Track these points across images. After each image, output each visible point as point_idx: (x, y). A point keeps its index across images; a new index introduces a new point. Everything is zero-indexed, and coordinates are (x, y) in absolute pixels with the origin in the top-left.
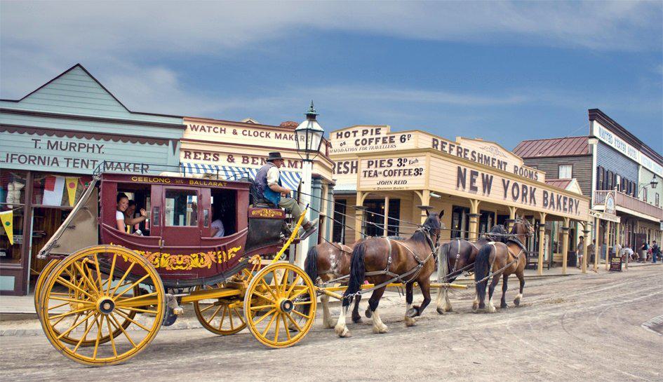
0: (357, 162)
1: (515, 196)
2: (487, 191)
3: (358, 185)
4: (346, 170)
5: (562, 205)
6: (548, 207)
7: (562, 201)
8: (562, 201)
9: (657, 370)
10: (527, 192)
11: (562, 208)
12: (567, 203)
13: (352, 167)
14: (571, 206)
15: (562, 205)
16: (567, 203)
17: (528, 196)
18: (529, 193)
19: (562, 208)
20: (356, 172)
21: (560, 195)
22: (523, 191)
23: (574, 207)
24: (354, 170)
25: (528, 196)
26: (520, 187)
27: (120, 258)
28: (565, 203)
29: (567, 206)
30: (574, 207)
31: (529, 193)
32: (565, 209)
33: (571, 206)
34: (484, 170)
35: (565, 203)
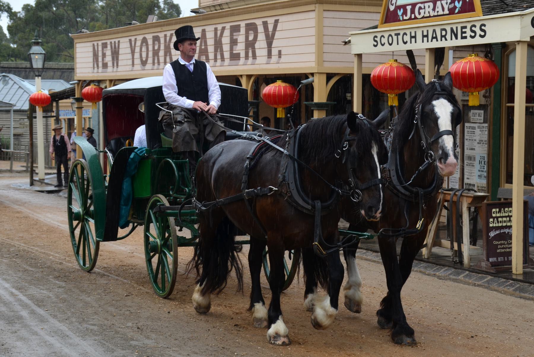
0: (415, 32)
1: (144, 59)
2: (115, 65)
3: (320, 60)
4: (473, 34)
5: (226, 48)
6: (242, 60)
7: (226, 40)
8: (226, 40)
9: (62, 222)
10: (159, 47)
11: (227, 55)
12: (241, 38)
13: (412, 37)
14: (250, 45)
15: (226, 48)
16: (241, 38)
17: (162, 53)
18: (162, 47)
19: (227, 55)
20: (416, 42)
21: (220, 27)
22: (154, 47)
23: (261, 44)
24: (413, 40)
25: (162, 53)
26: (150, 42)
27: (399, 89)
28: (234, 42)
29: (240, 48)
30: (261, 44)
31: (162, 47)
32: (235, 57)
33: (250, 45)
34: (103, 38)
35: (234, 42)
